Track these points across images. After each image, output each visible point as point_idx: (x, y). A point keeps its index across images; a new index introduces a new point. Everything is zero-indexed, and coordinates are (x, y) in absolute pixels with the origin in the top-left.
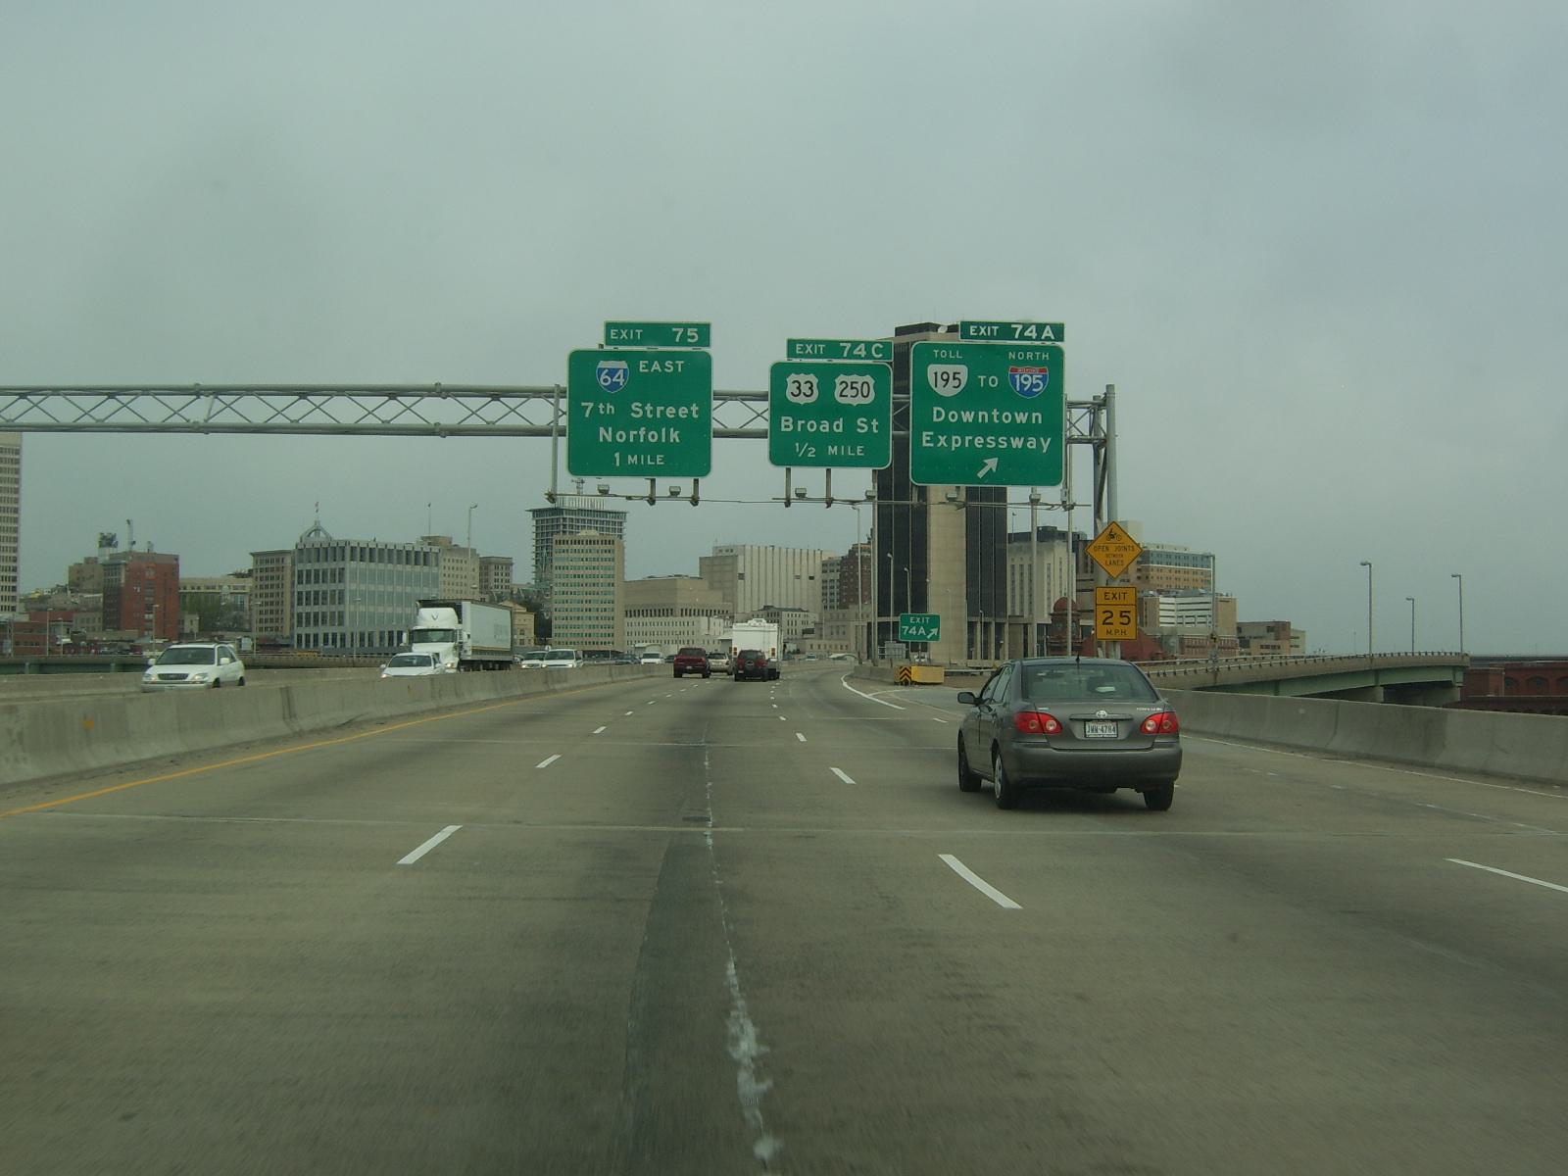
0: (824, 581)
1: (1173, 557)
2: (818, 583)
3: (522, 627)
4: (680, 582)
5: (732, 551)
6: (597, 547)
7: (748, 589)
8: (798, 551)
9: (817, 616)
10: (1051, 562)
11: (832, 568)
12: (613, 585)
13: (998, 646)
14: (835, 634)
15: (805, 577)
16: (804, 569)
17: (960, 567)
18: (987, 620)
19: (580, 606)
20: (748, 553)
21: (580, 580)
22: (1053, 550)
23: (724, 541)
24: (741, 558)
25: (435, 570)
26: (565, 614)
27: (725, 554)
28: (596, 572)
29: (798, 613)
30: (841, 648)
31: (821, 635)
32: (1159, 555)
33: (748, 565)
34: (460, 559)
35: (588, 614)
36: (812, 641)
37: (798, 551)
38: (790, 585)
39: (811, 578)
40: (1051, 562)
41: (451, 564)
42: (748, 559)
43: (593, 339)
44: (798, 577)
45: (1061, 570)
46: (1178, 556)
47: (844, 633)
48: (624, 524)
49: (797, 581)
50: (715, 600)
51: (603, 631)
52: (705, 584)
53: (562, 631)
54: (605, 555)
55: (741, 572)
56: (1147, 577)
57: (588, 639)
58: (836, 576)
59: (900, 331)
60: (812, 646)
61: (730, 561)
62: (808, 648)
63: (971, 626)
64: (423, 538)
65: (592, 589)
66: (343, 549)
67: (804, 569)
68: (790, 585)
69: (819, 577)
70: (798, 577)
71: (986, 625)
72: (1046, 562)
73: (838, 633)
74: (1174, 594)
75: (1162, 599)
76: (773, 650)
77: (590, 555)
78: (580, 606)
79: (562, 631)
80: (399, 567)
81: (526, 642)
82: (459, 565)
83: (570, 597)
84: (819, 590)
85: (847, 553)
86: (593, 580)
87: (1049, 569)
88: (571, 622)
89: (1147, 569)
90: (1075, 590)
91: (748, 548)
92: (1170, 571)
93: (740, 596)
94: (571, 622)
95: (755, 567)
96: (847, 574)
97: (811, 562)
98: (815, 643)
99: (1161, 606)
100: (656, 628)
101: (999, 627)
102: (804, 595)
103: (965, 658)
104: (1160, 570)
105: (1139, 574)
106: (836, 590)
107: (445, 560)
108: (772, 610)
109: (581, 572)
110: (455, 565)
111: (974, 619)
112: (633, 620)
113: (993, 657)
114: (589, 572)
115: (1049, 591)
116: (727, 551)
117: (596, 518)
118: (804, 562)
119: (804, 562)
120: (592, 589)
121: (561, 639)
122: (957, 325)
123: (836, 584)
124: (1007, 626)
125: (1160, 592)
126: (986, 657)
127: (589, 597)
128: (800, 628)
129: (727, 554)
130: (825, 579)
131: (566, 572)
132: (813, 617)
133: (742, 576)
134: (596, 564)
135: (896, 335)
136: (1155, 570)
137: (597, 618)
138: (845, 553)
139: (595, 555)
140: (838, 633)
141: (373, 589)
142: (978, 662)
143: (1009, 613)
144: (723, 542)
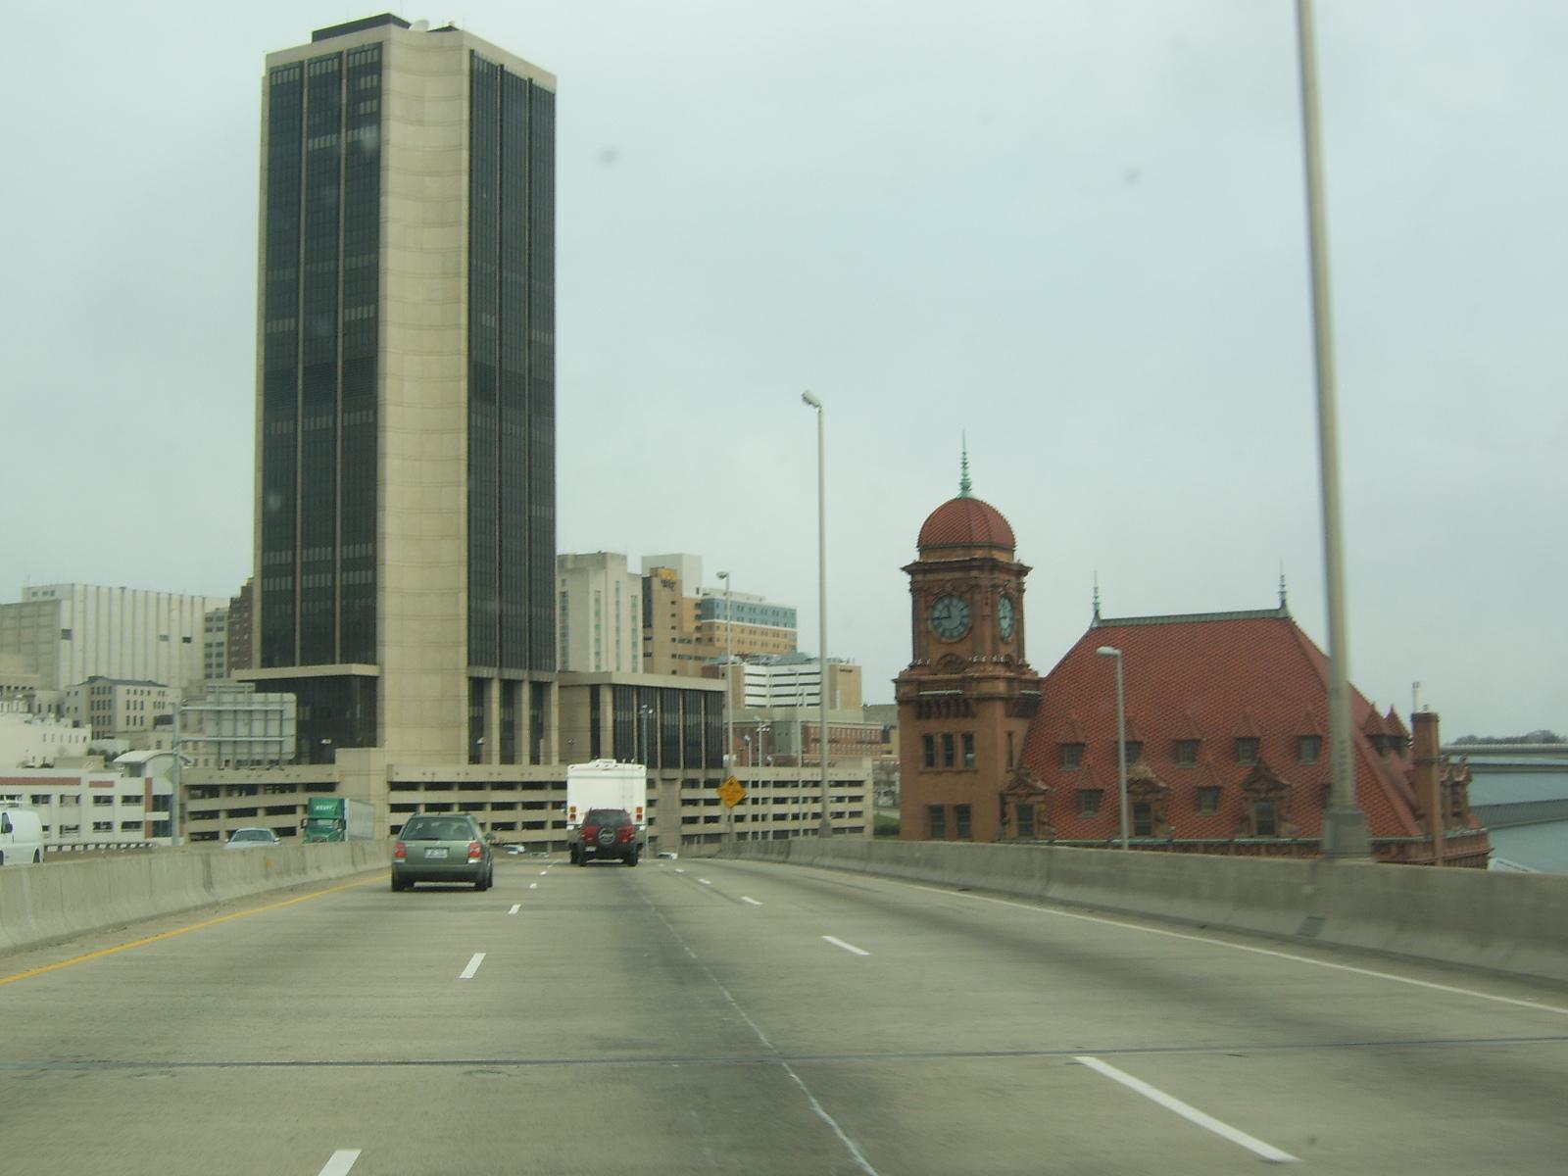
0: (208, 645)
2: (197, 649)
5: (53, 593)
9: (179, 692)
13: (538, 729)
15: (176, 639)
17: (454, 552)
18: (511, 674)
23: (42, 579)
24: (66, 605)
27: (41, 598)
29: (146, 689)
39: (187, 640)
43: (489, 889)
44: (165, 638)
45: (618, 603)
46: (753, 609)
49: (163, 644)
55: (66, 626)
56: (711, 640)
58: (222, 637)
59: (319, 36)
61: (47, 609)
63: (478, 687)
70: (165, 638)
71: (509, 688)
72: (593, 587)
74: (764, 660)
75: (748, 668)
84: (199, 660)
87: (597, 601)
89: (711, 626)
92: (743, 631)
95: (91, 617)
96: (237, 626)
97: (187, 614)
99: (748, 680)
101: (540, 690)
102: (177, 666)
103: (465, 758)
108: (97, 684)
111: (484, 672)
113: (526, 758)
115: (598, 640)
116: (45, 593)
118: (175, 614)
119: (175, 614)
122: (371, 658)
124: (555, 691)
125: (744, 657)
126: (508, 758)
128: (150, 713)
129: (46, 598)
130: (209, 641)
133: (67, 634)
135: (314, 40)
136: (722, 628)
138: (237, 593)
142: (493, 770)
143: (558, 669)
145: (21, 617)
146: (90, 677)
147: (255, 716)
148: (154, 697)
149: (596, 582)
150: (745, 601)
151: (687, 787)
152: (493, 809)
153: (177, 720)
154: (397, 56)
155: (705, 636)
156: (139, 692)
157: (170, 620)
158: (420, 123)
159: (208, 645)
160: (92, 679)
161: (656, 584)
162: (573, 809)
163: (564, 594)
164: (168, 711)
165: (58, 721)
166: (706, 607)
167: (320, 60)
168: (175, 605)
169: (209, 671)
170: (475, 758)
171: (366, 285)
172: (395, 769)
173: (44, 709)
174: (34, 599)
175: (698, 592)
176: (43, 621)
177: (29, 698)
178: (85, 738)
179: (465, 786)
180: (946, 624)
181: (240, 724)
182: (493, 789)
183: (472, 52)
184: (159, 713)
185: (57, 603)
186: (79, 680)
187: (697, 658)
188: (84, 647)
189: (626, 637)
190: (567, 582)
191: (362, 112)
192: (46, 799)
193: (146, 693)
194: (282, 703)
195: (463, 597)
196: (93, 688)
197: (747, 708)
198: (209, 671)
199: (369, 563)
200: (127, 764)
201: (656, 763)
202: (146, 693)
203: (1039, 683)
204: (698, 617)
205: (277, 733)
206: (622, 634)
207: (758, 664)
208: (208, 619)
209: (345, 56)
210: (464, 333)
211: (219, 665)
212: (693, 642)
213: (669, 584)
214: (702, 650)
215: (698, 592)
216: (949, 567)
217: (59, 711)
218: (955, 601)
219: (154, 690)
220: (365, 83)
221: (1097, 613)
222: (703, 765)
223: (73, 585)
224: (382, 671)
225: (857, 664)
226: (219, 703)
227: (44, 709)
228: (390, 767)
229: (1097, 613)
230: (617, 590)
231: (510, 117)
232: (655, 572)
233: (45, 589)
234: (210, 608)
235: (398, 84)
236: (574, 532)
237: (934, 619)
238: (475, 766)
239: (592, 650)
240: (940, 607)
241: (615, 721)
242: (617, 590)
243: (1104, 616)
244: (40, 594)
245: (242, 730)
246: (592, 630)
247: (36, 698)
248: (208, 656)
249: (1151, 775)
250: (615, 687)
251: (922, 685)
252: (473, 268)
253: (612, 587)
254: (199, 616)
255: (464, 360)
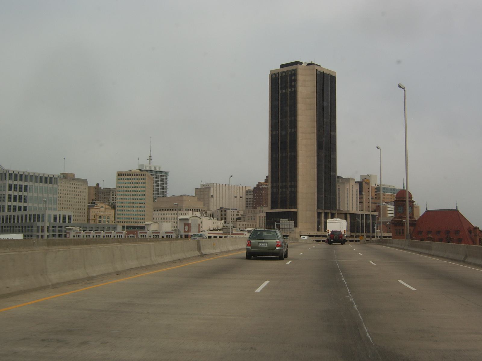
0: (247, 199)
1: (389, 189)
2: (244, 200)
3: (108, 215)
4: (184, 197)
6: (138, 177)
7: (215, 202)
8: (236, 186)
9: (243, 212)
10: (349, 187)
11: (250, 193)
12: (145, 195)
14: (250, 219)
15: (238, 197)
16: (238, 194)
17: (314, 184)
18: (326, 211)
19: (129, 205)
20: (215, 187)
21: (129, 193)
22: (349, 182)
24: (212, 189)
25: (55, 186)
26: (122, 208)
27: (205, 187)
28: (137, 189)
29: (234, 211)
30: (251, 226)
31: (244, 220)
32: (384, 189)
33: (215, 192)
34: (78, 184)
35: (133, 209)
36: (239, 222)
37: (236, 186)
38: (233, 200)
39: (241, 197)
40: (349, 187)
41: (73, 186)
42: (215, 189)
44: (236, 197)
45: (353, 191)
47: (254, 219)
48: (168, 177)
49: (235, 198)
50: (200, 205)
51: (140, 217)
52: (196, 199)
53: (120, 216)
54: (141, 181)
55: (212, 194)
57: (133, 220)
58: (251, 197)
59: (282, 66)
60: (240, 225)
61: (207, 190)
62: (238, 226)
63: (319, 214)
64: (61, 174)
65: (135, 197)
66: (5, 174)
67: (238, 194)
68: (233, 200)
69: (244, 197)
70: (236, 197)
73: (251, 219)
75: (389, 206)
76: (345, 231)
77: (134, 181)
78: (129, 205)
79: (120, 216)
80: (36, 184)
81: (111, 222)
82: (78, 186)
83: (124, 201)
85: (256, 186)
86: (135, 193)
87: (347, 190)
88: (124, 213)
90: (358, 202)
91: (215, 184)
92: (388, 195)
93: (211, 204)
94: (124, 213)
95: (218, 192)
97: (241, 191)
98: (241, 223)
100: (169, 216)
102: (238, 204)
103: (316, 230)
104: (384, 195)
105: (376, 197)
106: (251, 202)
107: (70, 184)
109: (130, 189)
110: (75, 186)
111: (320, 211)
112: (156, 212)
114: (133, 189)
116: (206, 186)
117: (156, 174)
118: (238, 191)
119: (238, 191)
120: (135, 197)
121: (120, 220)
123: (251, 200)
125: (387, 203)
127: (133, 201)
129: (206, 187)
131: (123, 189)
132: (241, 213)
133: (212, 196)
134: (137, 185)
137: (137, 211)
139: (137, 181)
140: (251, 219)
141: (31, 195)
143: (337, 209)
144: (205, 182)
145: (201, 192)
146: (220, 208)
147: (288, 224)
148: (236, 213)
149: (347, 186)
150: (389, 187)
151: (368, 237)
152: (322, 242)
153: (242, 219)
154: (300, 71)
155: (378, 197)
156: (233, 212)
157: (237, 192)
158: (305, 86)
159: (247, 199)
160: (221, 208)
161: (364, 183)
162: (328, 230)
163: (339, 189)
164: (240, 216)
165: (213, 219)
166: (378, 189)
167: (283, 72)
168: (238, 188)
169: (247, 205)
170: (318, 230)
171: (294, 124)
172: (302, 232)
173: (209, 216)
174: (203, 187)
175: (376, 185)
176: (206, 193)
177: (206, 213)
178: (222, 223)
179: (316, 236)
180: (400, 211)
181: (283, 226)
182: (322, 237)
183: (317, 70)
184: (237, 217)
185: (210, 188)
186: (218, 208)
187: (375, 203)
188: (216, 199)
189: (355, 199)
190: (340, 186)
191: (292, 84)
192: (222, 237)
193: (234, 212)
194: (292, 222)
195: (316, 194)
196: (221, 211)
197: (388, 217)
198: (247, 205)
199: (295, 186)
200: (247, 231)
201: (364, 232)
202: (234, 212)
203: (416, 221)
204: (376, 192)
205: (286, 227)
206: (354, 199)
207: (391, 205)
208: (246, 192)
209: (288, 71)
210: (316, 134)
211: (250, 204)
212: (374, 199)
213: (368, 183)
214: (376, 201)
215: (376, 185)
216: (400, 201)
217: (213, 216)
218: (401, 207)
219: (236, 211)
220: (293, 78)
221: (427, 209)
222: (371, 232)
223: (213, 183)
224: (298, 210)
225: (418, 205)
226: (282, 222)
227: (209, 216)
228: (300, 232)
229: (427, 209)
230: (352, 187)
231: (326, 83)
232: (363, 180)
233: (206, 185)
234: (247, 189)
235: (300, 78)
236: (342, 170)
237: (398, 210)
238: (319, 232)
239: (346, 203)
240: (399, 208)
241: (350, 222)
242: (352, 187)
243: (428, 209)
244: (205, 186)
245: (286, 227)
246: (346, 197)
247: (207, 213)
248: (247, 201)
249: (431, 236)
250: (350, 214)
251: (396, 221)
252: (318, 119)
253: (351, 186)
254: (244, 191)
255: (316, 140)
